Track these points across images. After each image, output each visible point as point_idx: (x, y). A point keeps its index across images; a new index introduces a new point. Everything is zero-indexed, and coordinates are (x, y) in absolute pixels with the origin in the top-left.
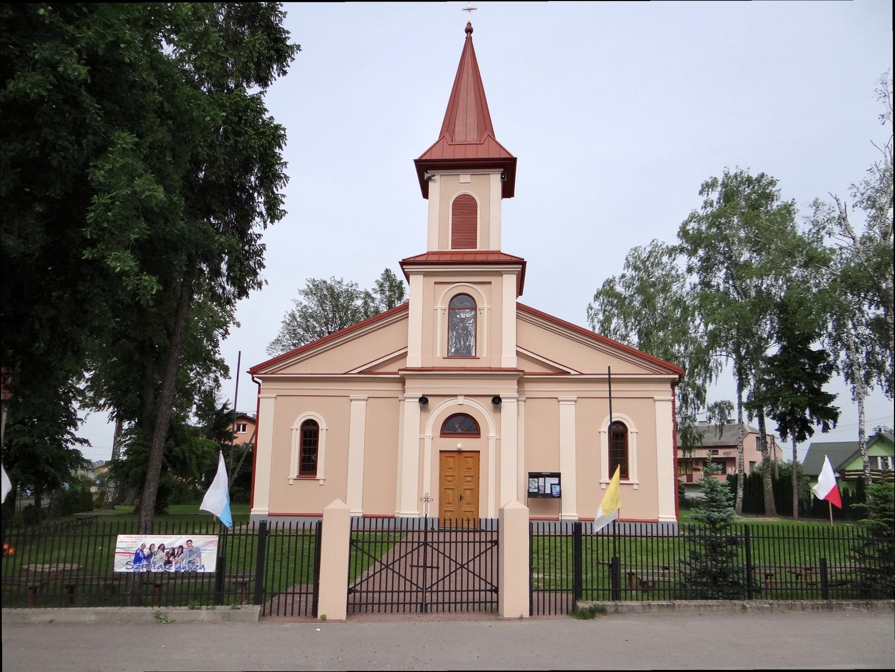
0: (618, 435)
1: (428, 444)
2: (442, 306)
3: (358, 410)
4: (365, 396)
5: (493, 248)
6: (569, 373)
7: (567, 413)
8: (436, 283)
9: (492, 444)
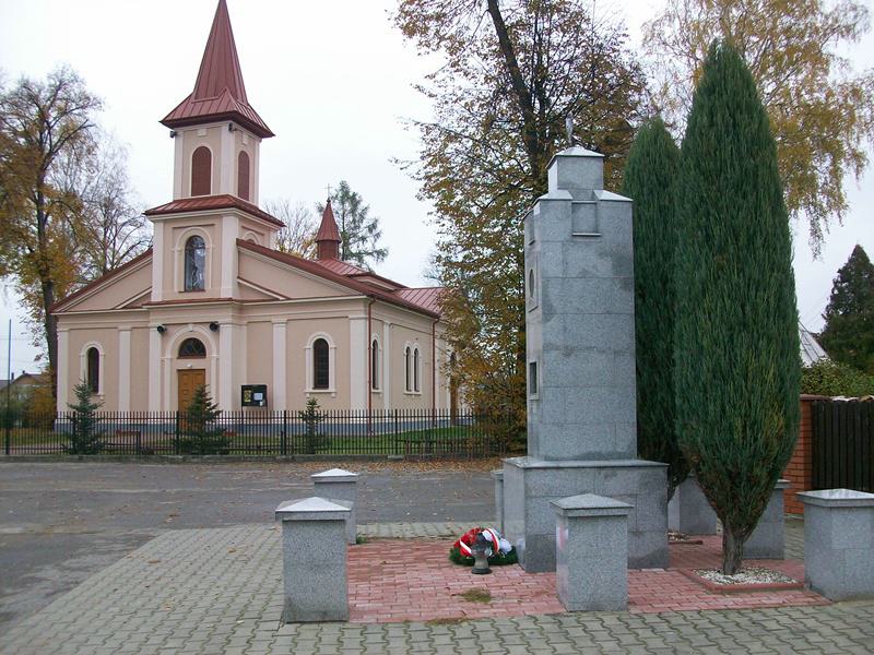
0: (321, 348)
1: (167, 363)
2: (180, 247)
3: (125, 337)
4: (129, 327)
5: (255, 204)
6: (278, 300)
7: (279, 333)
8: (174, 228)
9: (213, 362)
